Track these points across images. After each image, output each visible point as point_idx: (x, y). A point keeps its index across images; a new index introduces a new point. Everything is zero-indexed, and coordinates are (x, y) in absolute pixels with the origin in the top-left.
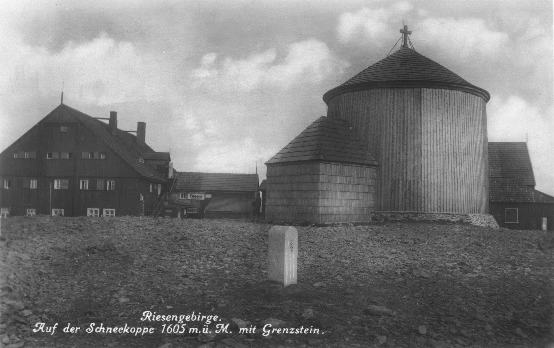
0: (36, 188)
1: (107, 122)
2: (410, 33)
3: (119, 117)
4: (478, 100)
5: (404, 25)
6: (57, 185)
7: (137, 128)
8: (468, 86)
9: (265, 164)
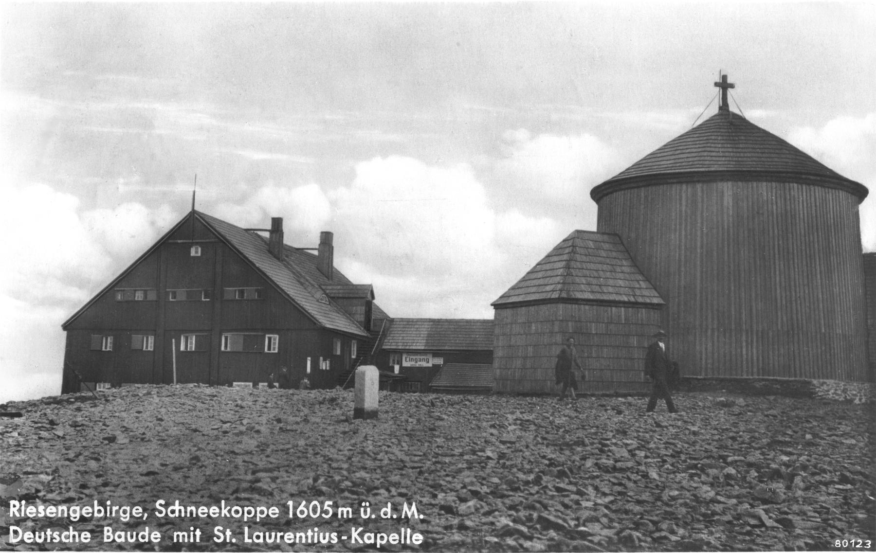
0: (152, 350)
1: (267, 235)
2: (732, 86)
3: (286, 228)
4: (842, 198)
5: (722, 74)
6: (662, 345)
7: (318, 242)
8: (202, 243)
9: (492, 305)
